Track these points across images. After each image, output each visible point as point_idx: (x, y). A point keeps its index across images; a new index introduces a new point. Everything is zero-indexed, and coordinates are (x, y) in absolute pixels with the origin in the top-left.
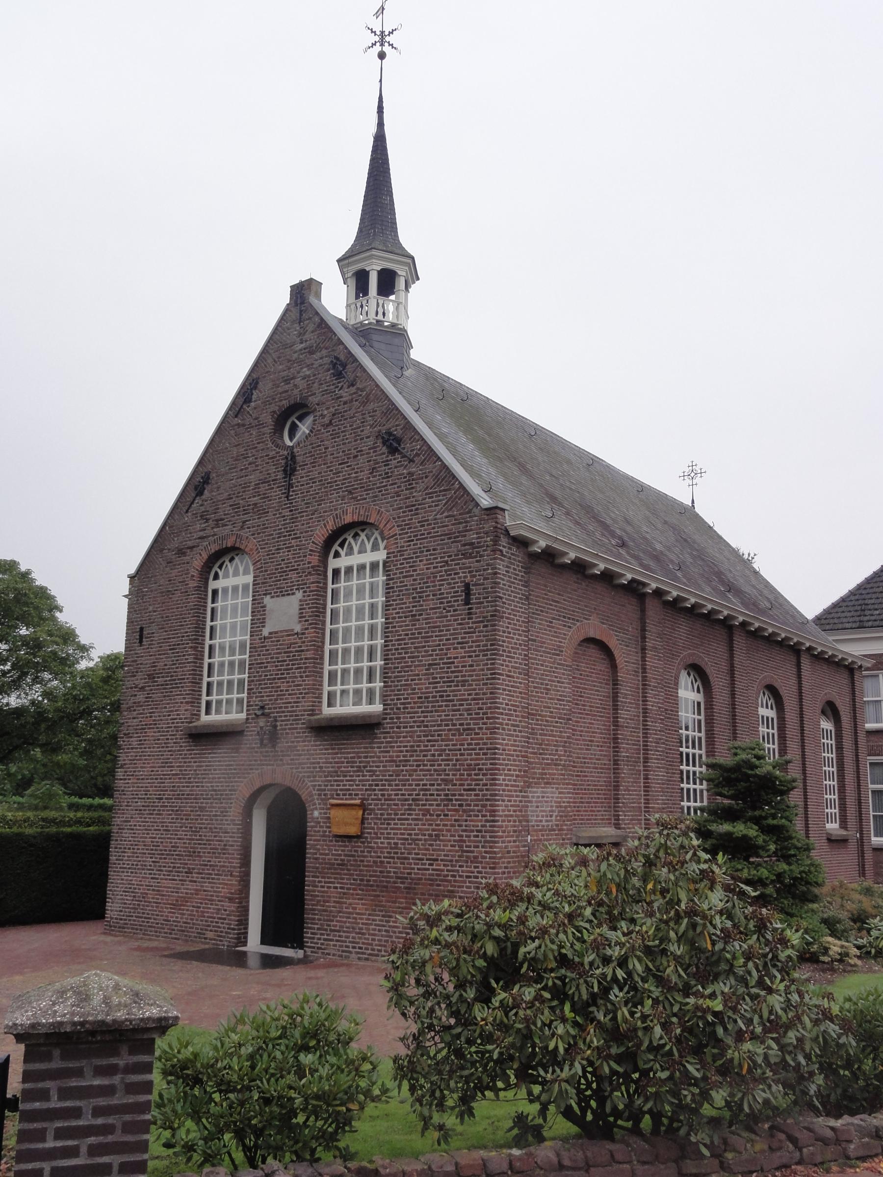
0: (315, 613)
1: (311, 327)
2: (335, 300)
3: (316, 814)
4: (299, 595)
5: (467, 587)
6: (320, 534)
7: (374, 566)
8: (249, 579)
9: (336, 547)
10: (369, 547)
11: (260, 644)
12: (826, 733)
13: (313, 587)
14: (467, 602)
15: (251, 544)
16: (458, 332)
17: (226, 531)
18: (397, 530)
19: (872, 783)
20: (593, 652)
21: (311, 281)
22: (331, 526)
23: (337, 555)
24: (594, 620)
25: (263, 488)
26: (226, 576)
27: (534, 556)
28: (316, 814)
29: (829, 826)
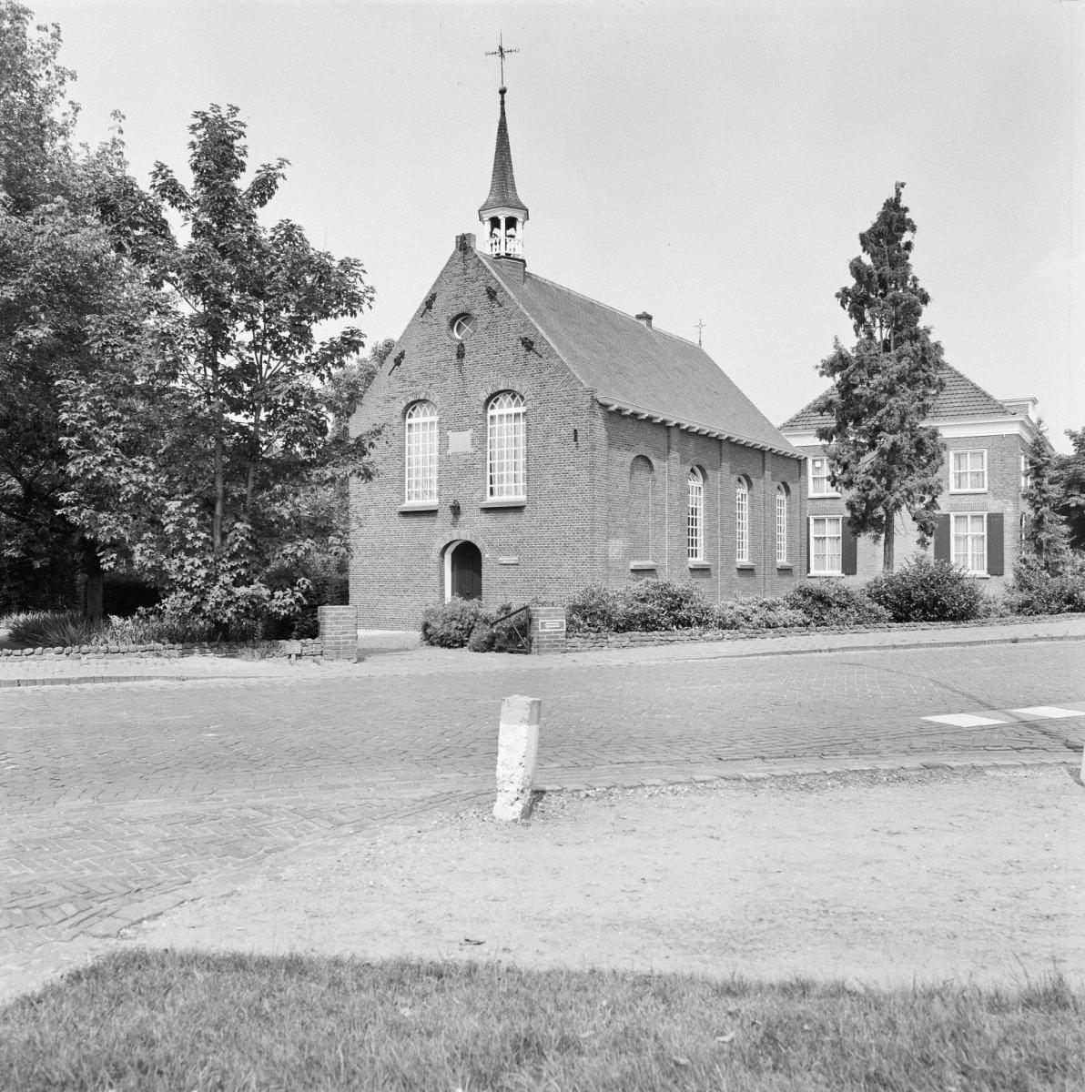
0: (481, 440)
1: (472, 265)
2: (483, 245)
3: (487, 556)
4: (471, 431)
5: (575, 431)
6: (484, 396)
7: (517, 415)
8: (435, 419)
9: (492, 403)
10: (513, 404)
11: (445, 460)
12: (781, 502)
13: (480, 427)
14: (576, 440)
15: (436, 398)
16: (550, 251)
17: (418, 389)
18: (532, 397)
19: (816, 568)
20: (641, 463)
21: (469, 235)
22: (490, 391)
23: (493, 407)
24: (642, 445)
25: (443, 364)
26: (418, 416)
27: (611, 413)
28: (487, 556)
29: (8, 553)
